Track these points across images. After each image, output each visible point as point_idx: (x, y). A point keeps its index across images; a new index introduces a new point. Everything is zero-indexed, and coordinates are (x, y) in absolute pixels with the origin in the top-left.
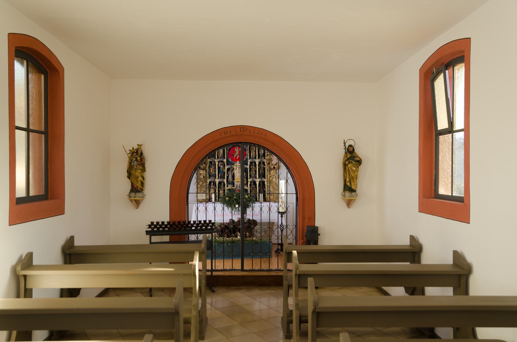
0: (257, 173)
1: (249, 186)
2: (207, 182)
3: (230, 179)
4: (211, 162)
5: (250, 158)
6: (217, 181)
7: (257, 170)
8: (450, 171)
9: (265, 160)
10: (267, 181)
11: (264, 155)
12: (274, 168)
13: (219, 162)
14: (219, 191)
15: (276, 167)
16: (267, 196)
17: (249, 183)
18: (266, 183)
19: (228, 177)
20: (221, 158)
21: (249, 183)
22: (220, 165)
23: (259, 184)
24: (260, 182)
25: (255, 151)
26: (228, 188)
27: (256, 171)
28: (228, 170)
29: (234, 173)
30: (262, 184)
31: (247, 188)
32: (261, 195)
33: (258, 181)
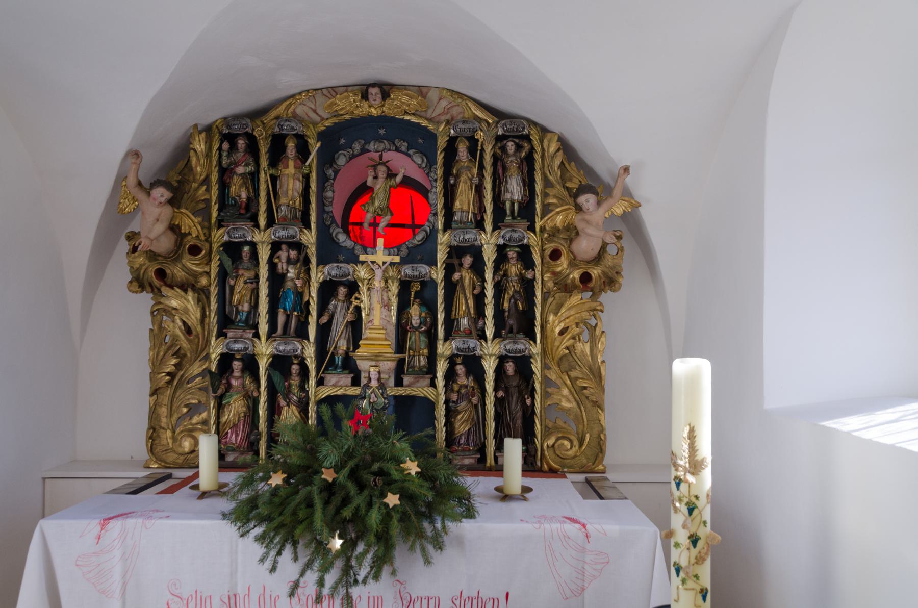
0: (489, 312)
1: (440, 382)
2: (207, 357)
3: (340, 342)
4: (232, 249)
5: (447, 226)
6: (265, 350)
7: (490, 292)
8: (882, 427)
9: (532, 239)
10: (544, 352)
11: (527, 211)
12: (586, 278)
13: (276, 247)
14: (274, 410)
15: (595, 272)
16: (544, 442)
17: (441, 367)
18: (536, 367)
19: (324, 331)
20: (286, 223)
21: (441, 367)
22: (282, 266)
23: (500, 371)
24: (502, 359)
25: (479, 189)
26: (325, 392)
27: (480, 299)
28: (328, 289)
29: (358, 309)
30: (518, 375)
31: (428, 393)
32: (514, 448)
33: (490, 353)
